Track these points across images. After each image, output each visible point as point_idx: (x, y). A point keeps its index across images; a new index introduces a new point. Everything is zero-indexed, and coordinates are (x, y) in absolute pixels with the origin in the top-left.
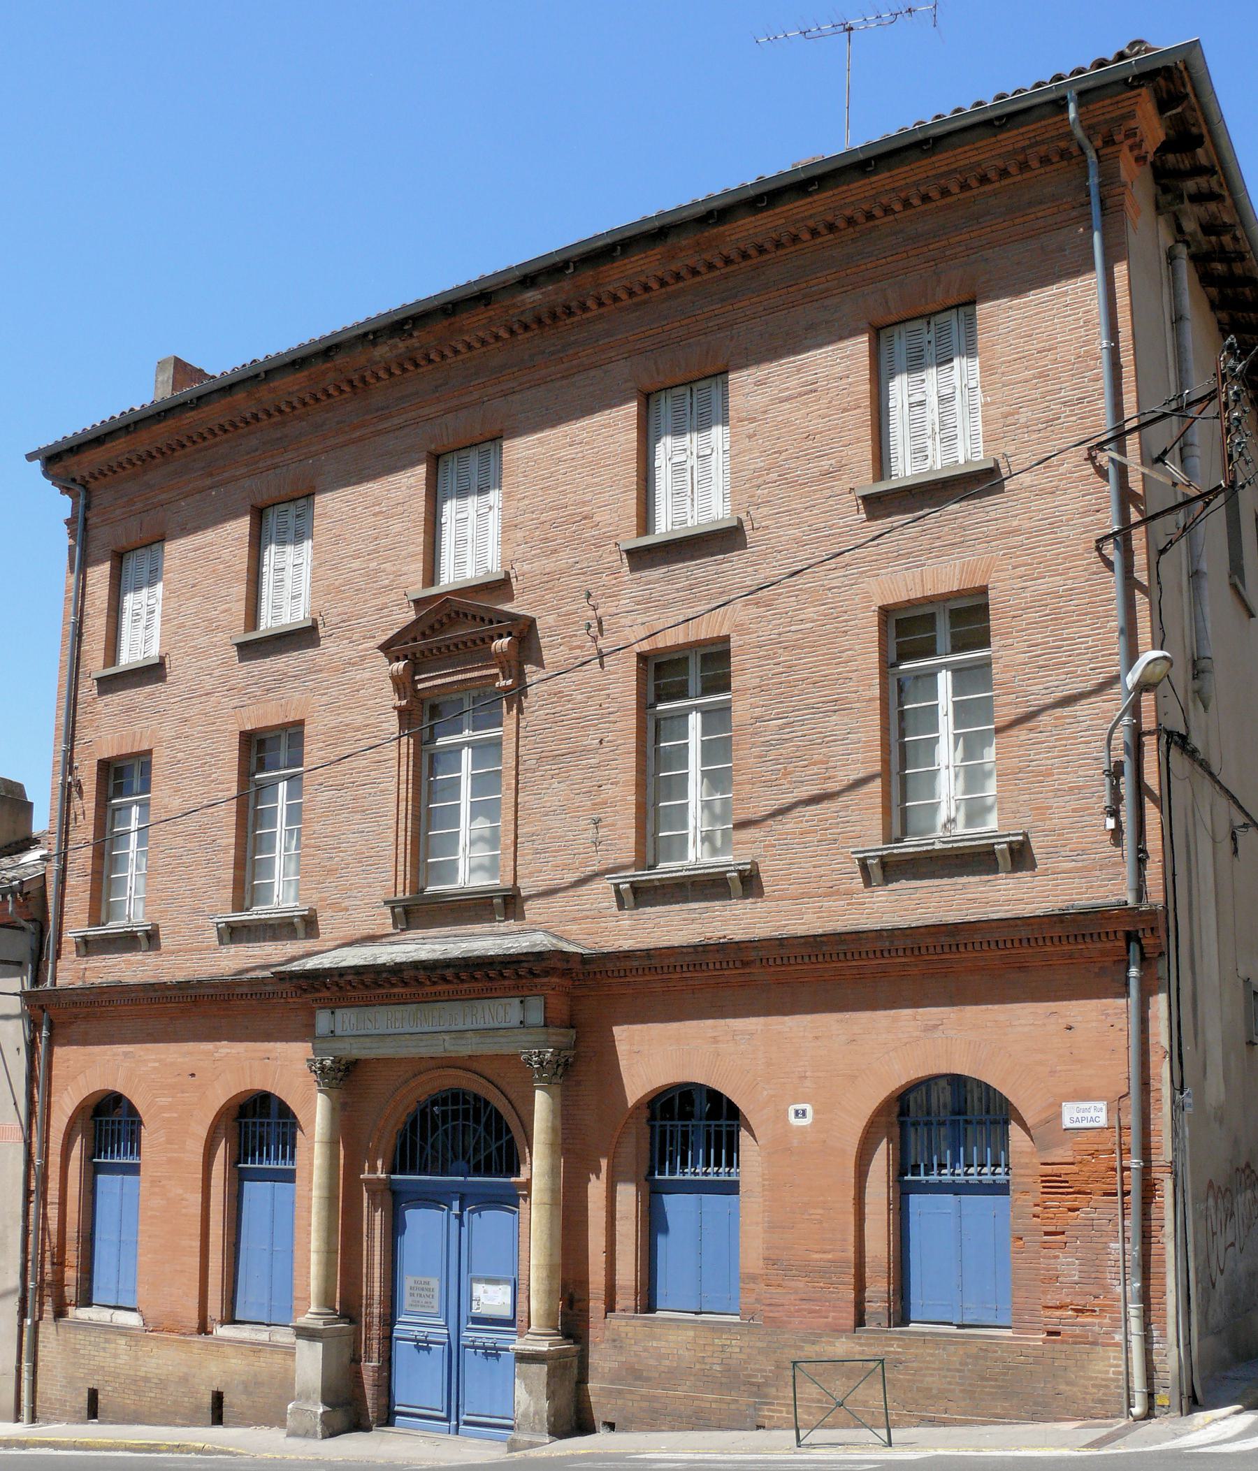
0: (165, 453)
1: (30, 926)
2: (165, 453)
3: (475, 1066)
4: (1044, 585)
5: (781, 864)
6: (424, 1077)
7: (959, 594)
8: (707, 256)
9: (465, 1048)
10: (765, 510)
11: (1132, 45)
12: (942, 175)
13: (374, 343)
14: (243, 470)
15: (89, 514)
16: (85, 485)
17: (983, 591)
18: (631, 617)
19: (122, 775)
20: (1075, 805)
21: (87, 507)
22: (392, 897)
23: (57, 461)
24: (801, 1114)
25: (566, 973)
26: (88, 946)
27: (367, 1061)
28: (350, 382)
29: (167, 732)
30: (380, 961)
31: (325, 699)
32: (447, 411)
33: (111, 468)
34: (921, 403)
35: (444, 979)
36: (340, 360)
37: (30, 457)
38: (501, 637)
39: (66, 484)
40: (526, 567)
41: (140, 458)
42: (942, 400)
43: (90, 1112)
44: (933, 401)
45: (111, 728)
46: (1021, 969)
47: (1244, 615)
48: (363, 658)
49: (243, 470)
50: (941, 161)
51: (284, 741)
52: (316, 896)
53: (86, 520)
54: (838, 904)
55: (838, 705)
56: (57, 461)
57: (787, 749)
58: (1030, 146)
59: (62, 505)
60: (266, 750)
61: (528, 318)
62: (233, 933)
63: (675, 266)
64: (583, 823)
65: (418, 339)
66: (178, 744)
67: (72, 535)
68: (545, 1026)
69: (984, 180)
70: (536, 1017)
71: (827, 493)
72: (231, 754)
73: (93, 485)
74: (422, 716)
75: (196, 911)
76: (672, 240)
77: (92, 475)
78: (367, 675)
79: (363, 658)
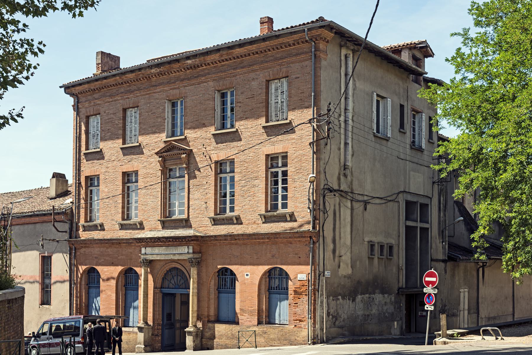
0: (100, 89)
1: (69, 222)
2: (100, 89)
3: (179, 262)
4: (298, 153)
5: (244, 216)
6: (167, 265)
7: (283, 153)
8: (230, 57)
9: (176, 257)
10: (242, 127)
11: (319, 18)
12: (281, 43)
13: (151, 69)
14: (120, 98)
15: (79, 104)
16: (77, 96)
17: (287, 152)
18: (214, 151)
19: (92, 181)
20: (302, 206)
21: (78, 102)
22: (160, 219)
23: (68, 88)
24: (247, 275)
25: (197, 240)
26: (85, 229)
27: (155, 260)
28: (146, 78)
29: (103, 170)
30: (155, 236)
31: (143, 165)
32: (171, 89)
33: (84, 92)
34: (277, 102)
35: (170, 241)
36: (143, 71)
37: (61, 87)
38: (184, 154)
39: (72, 95)
40: (190, 135)
41: (92, 90)
42: (282, 102)
43: (87, 272)
44: (280, 102)
45: (88, 168)
46: (291, 243)
47: (403, 134)
48: (152, 155)
49: (120, 98)
50: (281, 40)
51: (134, 175)
52: (142, 217)
53: (78, 106)
54: (255, 226)
55: (256, 178)
56: (68, 88)
57: (246, 188)
58: (300, 39)
59: (71, 100)
60: (128, 178)
61: (189, 67)
62: (123, 227)
63: (223, 58)
64: (203, 203)
65: (162, 69)
66: (106, 174)
67: (74, 110)
68: (193, 253)
69: (290, 46)
70: (191, 251)
71: (256, 124)
72: (120, 178)
73: (79, 96)
74: (167, 172)
75: (112, 220)
76: (221, 52)
77: (79, 93)
78: (153, 160)
79: (152, 155)
